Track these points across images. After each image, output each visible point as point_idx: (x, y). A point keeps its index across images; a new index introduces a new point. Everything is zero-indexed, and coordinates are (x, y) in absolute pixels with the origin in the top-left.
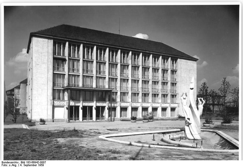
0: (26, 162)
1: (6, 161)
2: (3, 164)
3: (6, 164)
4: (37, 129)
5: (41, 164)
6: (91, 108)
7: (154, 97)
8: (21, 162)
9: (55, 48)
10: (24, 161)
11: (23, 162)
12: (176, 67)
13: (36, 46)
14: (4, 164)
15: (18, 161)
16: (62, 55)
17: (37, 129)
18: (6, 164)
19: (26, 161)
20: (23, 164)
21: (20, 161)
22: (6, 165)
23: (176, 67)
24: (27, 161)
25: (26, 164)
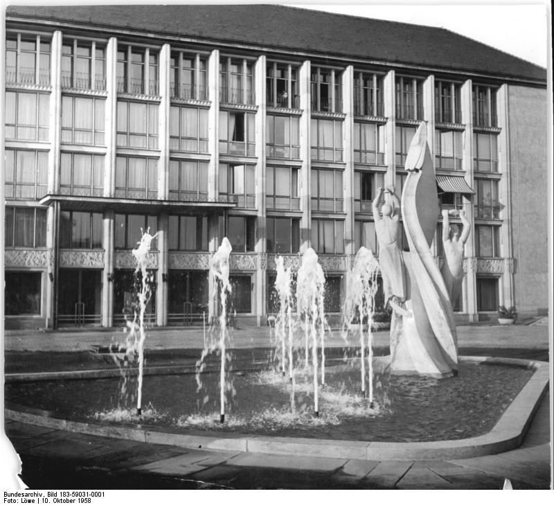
0: (59, 495)
1: (32, 491)
2: (7, 497)
3: (13, 498)
4: (122, 417)
5: (84, 498)
6: (77, 314)
7: (94, 314)
8: (49, 495)
9: (381, 158)
10: (55, 491)
11: (53, 495)
12: (270, 151)
13: (297, 383)
14: (10, 498)
15: (40, 491)
16: (375, 115)
17: (122, 417)
18: (13, 498)
19: (59, 491)
20: (51, 499)
21: (44, 492)
22: (15, 501)
23: (270, 151)
24: (63, 491)
25: (59, 497)
